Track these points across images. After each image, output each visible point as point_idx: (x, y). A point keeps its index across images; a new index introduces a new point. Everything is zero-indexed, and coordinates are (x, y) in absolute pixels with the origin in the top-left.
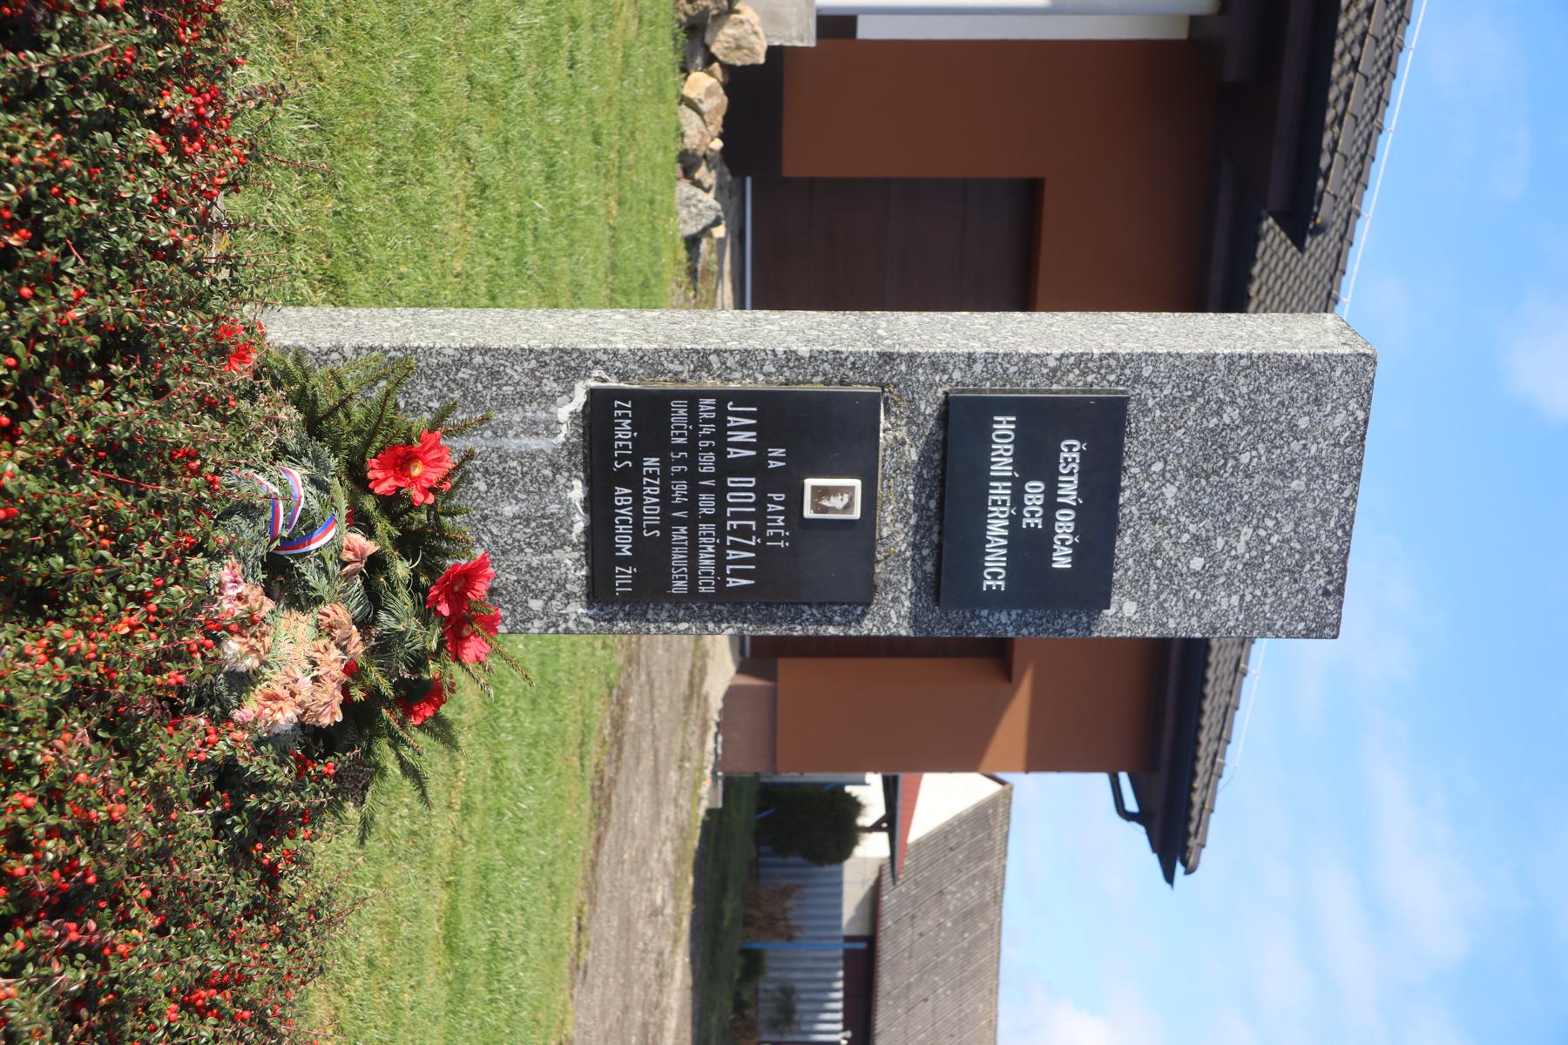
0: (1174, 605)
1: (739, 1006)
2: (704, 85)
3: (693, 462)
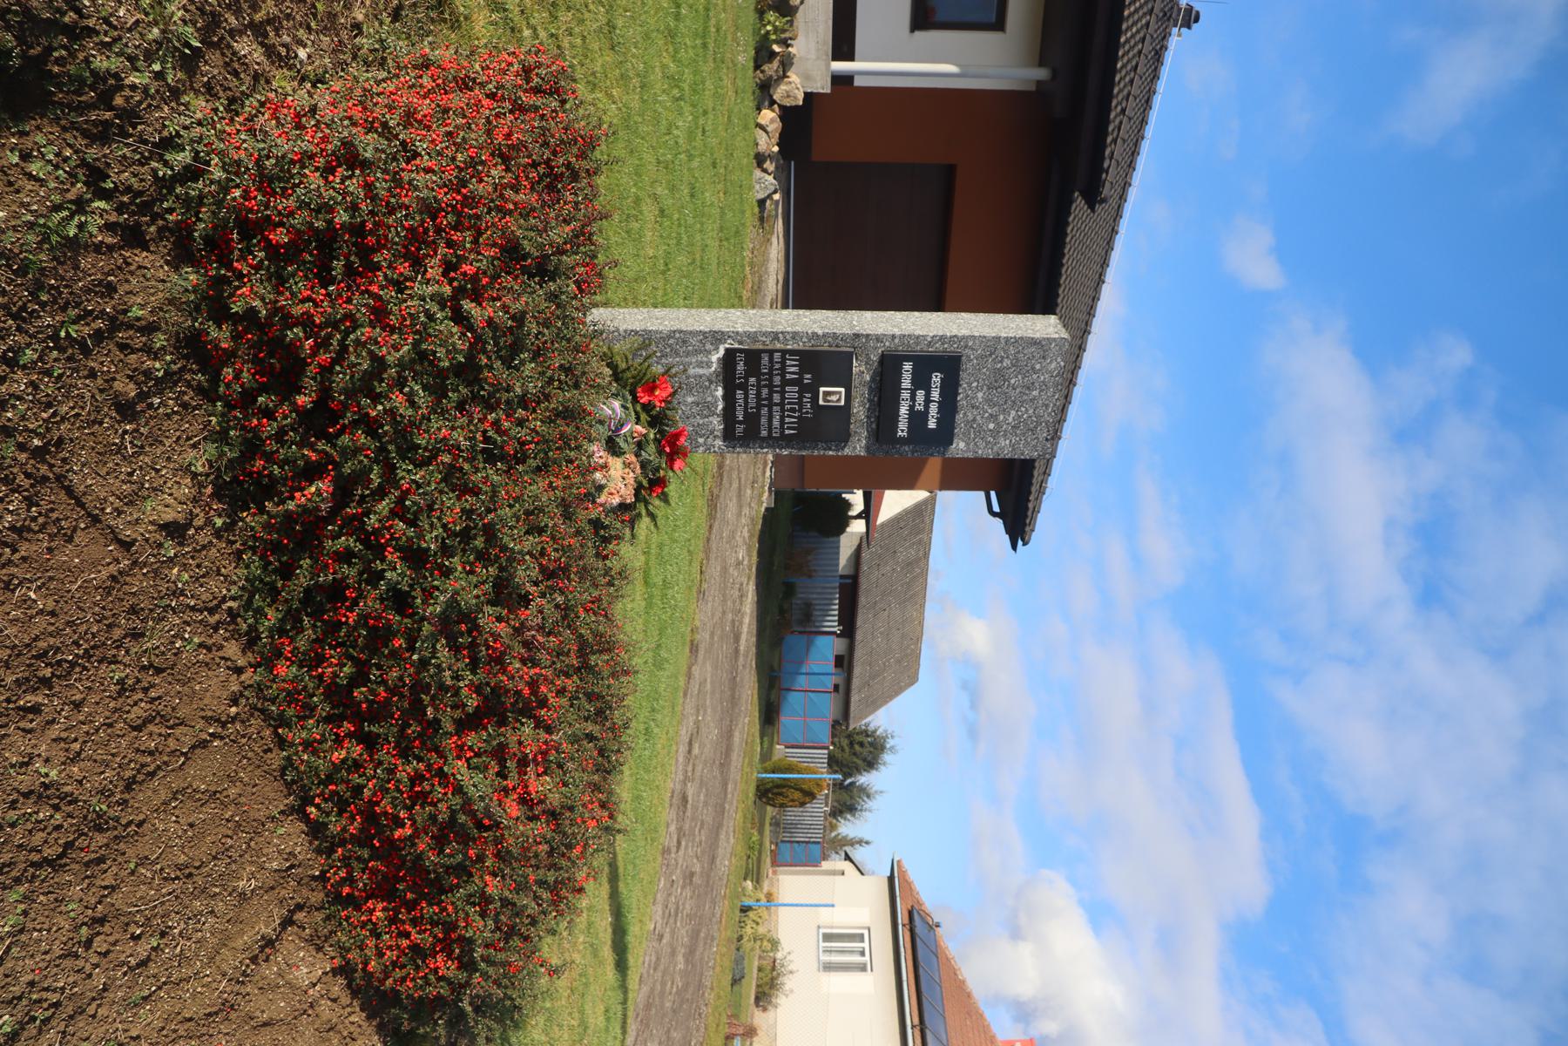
0: (982, 444)
1: (782, 612)
2: (768, 116)
3: (771, 380)
